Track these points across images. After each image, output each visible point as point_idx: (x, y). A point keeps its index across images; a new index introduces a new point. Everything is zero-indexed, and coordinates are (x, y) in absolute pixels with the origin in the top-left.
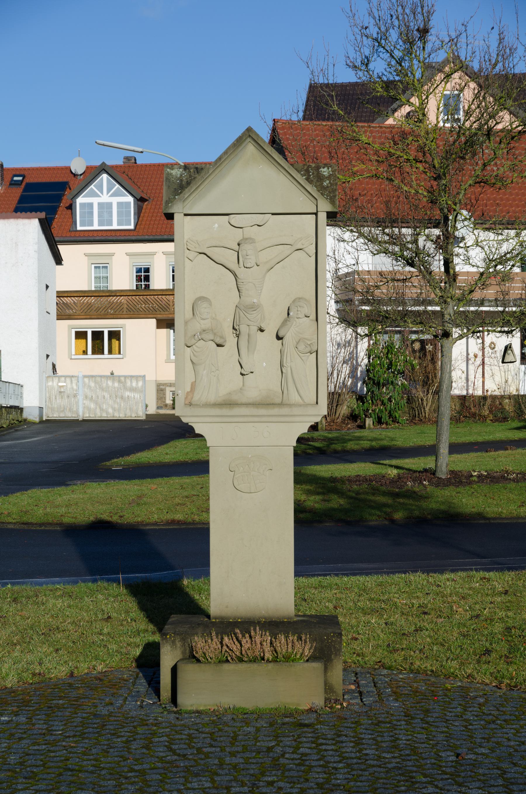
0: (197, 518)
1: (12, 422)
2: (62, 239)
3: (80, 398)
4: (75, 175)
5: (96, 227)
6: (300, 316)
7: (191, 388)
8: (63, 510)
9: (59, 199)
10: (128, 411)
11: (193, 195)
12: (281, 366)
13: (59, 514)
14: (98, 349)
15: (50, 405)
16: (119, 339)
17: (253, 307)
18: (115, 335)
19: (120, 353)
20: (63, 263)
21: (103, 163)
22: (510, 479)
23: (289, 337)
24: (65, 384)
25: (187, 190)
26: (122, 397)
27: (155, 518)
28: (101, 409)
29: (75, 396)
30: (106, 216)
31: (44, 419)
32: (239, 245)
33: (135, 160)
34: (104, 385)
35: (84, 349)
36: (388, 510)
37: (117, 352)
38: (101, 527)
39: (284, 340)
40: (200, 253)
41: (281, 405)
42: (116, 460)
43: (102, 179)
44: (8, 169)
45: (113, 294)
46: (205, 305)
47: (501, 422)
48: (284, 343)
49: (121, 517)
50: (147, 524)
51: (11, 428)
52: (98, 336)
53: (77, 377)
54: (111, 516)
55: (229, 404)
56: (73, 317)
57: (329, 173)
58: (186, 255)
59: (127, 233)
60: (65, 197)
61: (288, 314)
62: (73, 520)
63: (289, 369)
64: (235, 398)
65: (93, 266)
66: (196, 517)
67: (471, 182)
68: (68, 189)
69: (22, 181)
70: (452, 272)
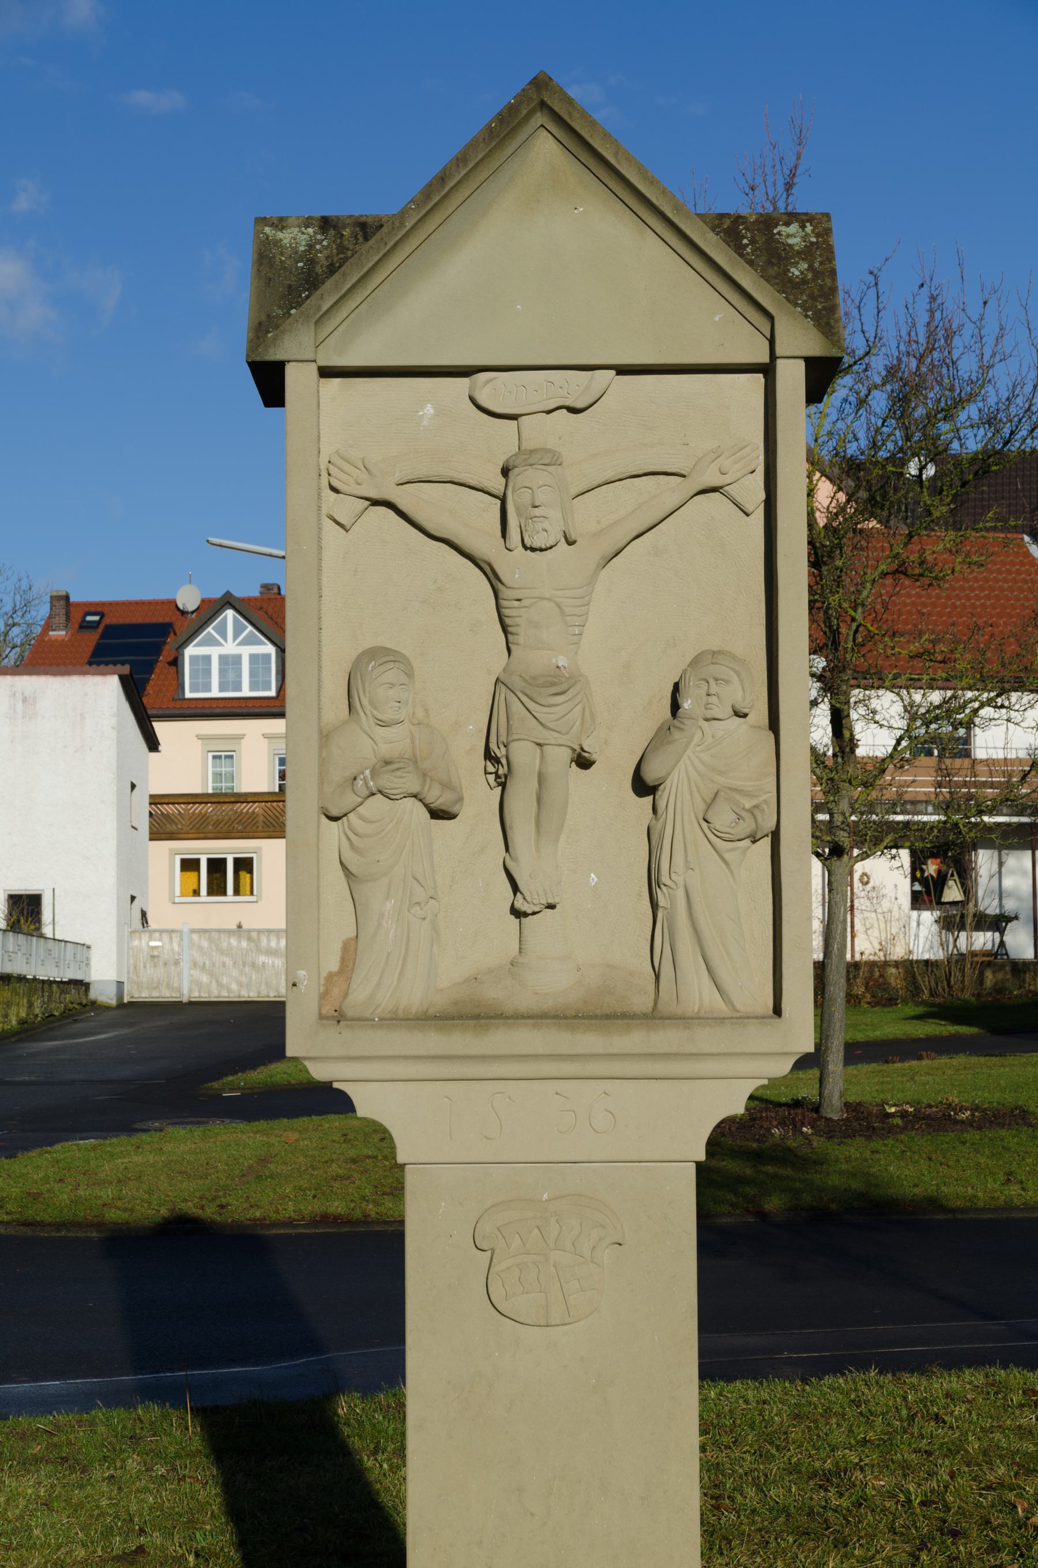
0: (371, 1209)
1: (70, 1006)
2: (161, 712)
3: (185, 965)
4: (183, 613)
5: (215, 693)
6: (716, 713)
7: (343, 960)
8: (108, 1193)
9: (157, 649)
10: (263, 987)
11: (351, 304)
12: (653, 882)
13: (100, 1202)
14: (217, 888)
15: (135, 978)
16: (250, 871)
17: (558, 683)
18: (244, 865)
19: (252, 893)
20: (160, 748)
21: (228, 593)
22: (962, 1122)
23: (682, 778)
24: (159, 944)
25: (328, 284)
26: (253, 965)
27: (289, 1210)
28: (220, 985)
29: (176, 963)
30: (231, 676)
31: (126, 1001)
32: (505, 472)
33: (279, 589)
34: (225, 945)
35: (196, 887)
36: (750, 1191)
37: (248, 892)
38: (182, 1231)
39: (662, 796)
40: (376, 503)
41: (654, 1017)
42: (230, 1078)
43: (225, 618)
44: (78, 604)
45: (241, 800)
46: (392, 674)
47: (884, 1006)
48: (661, 805)
49: (222, 1207)
50: (274, 1225)
51: (67, 1017)
52: (217, 866)
53: (180, 932)
54: (202, 1208)
55: (470, 1014)
56: (181, 836)
57: (805, 238)
58: (325, 510)
59: (265, 703)
60: (167, 647)
61: (675, 707)
62: (126, 1215)
63: (680, 893)
64: (493, 993)
65: (210, 755)
66: (371, 1206)
67: (883, 567)
68: (172, 635)
69: (99, 622)
70: (847, 734)
